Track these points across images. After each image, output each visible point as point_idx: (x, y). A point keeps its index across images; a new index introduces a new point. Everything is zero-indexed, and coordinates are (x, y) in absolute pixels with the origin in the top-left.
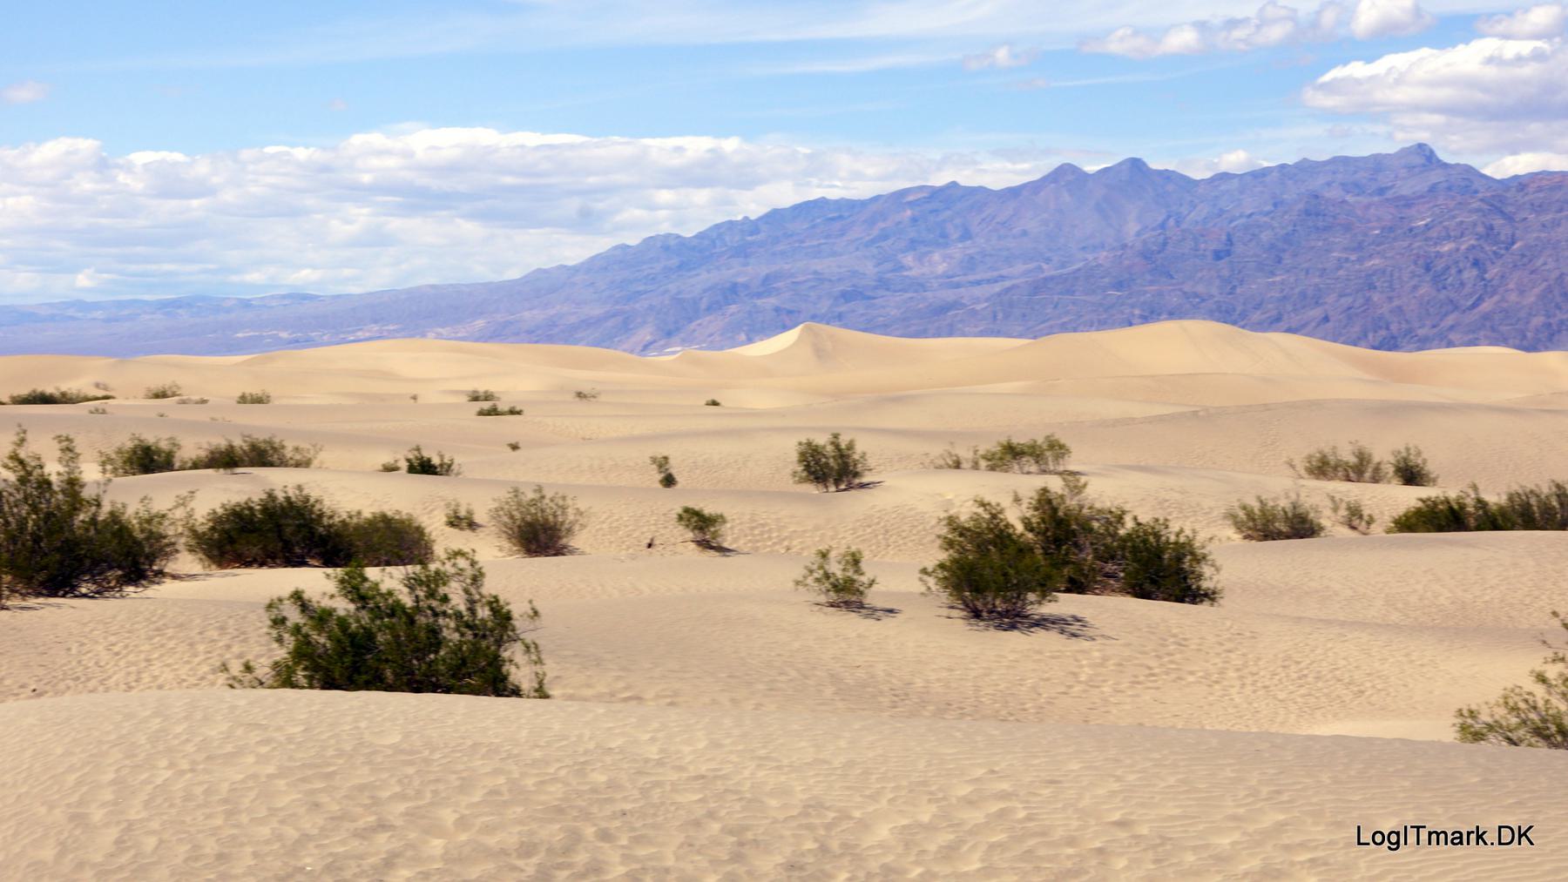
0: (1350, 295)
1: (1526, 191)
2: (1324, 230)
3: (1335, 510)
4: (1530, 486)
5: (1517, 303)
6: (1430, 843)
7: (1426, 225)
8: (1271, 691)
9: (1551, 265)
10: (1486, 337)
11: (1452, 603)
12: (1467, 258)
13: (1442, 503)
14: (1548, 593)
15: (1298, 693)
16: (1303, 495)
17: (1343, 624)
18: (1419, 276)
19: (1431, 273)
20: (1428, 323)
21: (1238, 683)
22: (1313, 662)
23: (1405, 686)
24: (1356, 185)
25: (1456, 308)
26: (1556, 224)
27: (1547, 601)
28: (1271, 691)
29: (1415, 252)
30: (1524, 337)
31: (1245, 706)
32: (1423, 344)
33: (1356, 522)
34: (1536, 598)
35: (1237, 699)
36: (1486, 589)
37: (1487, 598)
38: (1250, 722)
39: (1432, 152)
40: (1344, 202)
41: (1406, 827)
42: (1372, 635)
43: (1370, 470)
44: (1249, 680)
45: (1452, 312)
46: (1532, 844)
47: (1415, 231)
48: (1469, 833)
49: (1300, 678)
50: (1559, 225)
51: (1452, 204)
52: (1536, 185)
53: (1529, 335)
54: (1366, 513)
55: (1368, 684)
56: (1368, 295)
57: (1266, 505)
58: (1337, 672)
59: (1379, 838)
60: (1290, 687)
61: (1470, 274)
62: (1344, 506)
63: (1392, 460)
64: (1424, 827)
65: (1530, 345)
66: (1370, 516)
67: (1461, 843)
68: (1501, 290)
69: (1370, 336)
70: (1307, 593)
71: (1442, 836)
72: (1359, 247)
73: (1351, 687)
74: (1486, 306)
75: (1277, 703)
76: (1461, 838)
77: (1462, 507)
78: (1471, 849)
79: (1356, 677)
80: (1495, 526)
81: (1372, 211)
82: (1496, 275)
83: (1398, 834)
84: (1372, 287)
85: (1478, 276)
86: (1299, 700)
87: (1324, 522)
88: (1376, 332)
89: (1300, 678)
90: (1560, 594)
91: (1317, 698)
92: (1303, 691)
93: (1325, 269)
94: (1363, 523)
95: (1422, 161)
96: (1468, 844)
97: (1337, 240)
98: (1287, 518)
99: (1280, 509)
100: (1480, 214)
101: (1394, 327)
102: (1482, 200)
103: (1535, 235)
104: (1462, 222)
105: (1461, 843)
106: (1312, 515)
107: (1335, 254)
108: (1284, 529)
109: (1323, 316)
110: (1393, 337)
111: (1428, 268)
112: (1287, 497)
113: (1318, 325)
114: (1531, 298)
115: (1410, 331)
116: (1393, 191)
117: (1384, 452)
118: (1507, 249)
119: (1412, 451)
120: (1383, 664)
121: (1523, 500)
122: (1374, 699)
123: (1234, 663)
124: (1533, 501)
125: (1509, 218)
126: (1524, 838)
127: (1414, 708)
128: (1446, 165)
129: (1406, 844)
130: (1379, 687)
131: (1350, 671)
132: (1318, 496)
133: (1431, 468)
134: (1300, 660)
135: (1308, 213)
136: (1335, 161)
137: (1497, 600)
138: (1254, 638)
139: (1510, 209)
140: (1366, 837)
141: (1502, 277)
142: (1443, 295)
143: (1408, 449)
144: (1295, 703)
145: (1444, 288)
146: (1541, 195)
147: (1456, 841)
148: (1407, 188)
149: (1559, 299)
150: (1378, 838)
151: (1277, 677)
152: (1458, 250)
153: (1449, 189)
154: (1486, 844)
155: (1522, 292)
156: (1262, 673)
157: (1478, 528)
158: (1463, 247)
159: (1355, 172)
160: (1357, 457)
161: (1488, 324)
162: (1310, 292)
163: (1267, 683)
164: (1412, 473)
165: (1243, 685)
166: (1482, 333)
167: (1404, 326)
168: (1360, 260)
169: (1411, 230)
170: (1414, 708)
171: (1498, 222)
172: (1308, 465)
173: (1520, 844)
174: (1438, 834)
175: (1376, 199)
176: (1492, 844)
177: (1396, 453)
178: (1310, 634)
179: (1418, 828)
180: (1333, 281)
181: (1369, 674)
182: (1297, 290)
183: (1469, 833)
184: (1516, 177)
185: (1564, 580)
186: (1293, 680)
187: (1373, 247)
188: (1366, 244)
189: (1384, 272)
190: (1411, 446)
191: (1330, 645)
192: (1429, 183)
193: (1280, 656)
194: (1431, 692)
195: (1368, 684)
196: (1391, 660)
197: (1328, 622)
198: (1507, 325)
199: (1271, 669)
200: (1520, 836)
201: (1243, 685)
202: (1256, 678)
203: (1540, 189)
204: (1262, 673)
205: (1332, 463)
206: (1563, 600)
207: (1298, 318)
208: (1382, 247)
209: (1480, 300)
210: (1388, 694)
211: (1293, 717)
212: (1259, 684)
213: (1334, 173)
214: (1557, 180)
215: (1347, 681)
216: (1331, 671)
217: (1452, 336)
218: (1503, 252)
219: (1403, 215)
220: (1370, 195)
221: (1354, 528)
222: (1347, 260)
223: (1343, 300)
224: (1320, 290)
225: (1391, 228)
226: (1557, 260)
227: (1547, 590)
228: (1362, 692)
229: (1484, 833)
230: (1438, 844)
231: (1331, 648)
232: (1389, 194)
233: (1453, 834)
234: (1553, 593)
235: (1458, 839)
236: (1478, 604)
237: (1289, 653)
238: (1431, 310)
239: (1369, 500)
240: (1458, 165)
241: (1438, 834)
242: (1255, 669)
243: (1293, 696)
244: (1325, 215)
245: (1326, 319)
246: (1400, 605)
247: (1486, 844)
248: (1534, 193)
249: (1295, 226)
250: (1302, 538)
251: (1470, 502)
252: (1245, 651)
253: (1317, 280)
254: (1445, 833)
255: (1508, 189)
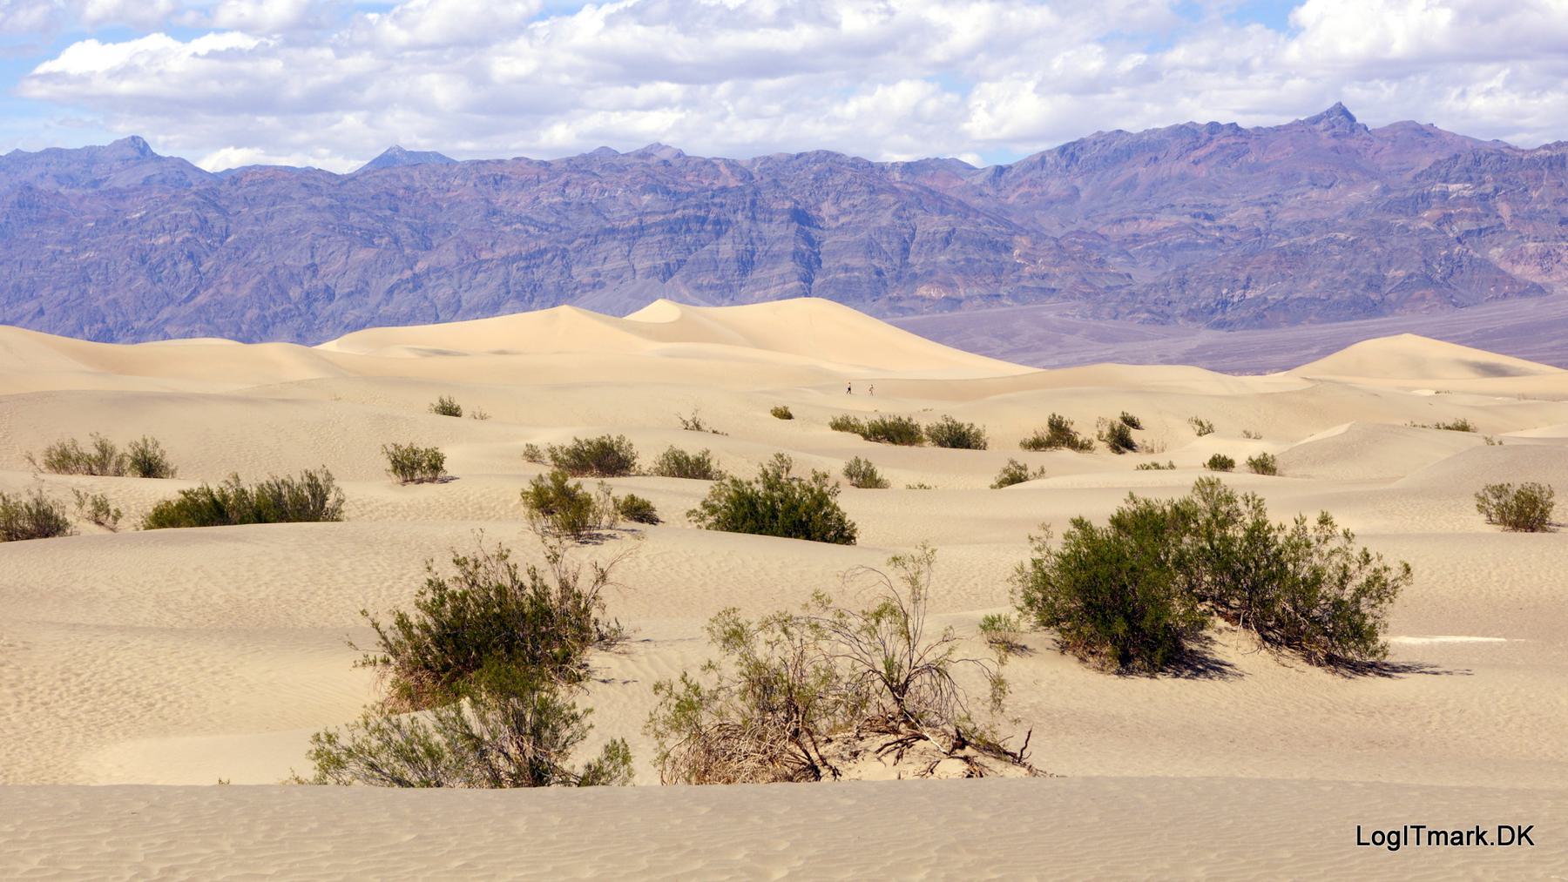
0: (66, 287)
1: (239, 185)
2: (38, 222)
3: (81, 505)
4: (282, 476)
5: (232, 295)
6: (1430, 843)
7: (141, 218)
8: (52, 708)
9: (264, 258)
10: (201, 330)
11: (226, 601)
12: (182, 251)
13: (204, 494)
14: (324, 587)
15: (83, 709)
16: (44, 490)
17: (122, 629)
18: (135, 269)
19: (147, 265)
20: (144, 315)
21: (14, 701)
22: (95, 674)
23: (198, 696)
24: (70, 177)
25: (171, 300)
26: (269, 217)
27: (324, 596)
28: (52, 708)
29: (130, 244)
30: (240, 329)
31: (25, 726)
32: (139, 336)
33: (102, 518)
34: (312, 593)
35: (13, 719)
36: (260, 586)
37: (262, 595)
38: (32, 745)
39: (146, 145)
40: (58, 193)
41: (1406, 827)
42: (156, 641)
43: (113, 463)
44: (25, 698)
45: (168, 304)
46: (1532, 844)
47: (130, 223)
48: (1469, 833)
49: (82, 692)
50: (272, 218)
51: (167, 197)
52: (248, 179)
53: (244, 327)
54: (112, 508)
55: (158, 696)
56: (83, 287)
57: (9, 501)
58: (123, 684)
59: (1379, 838)
60: (72, 703)
61: (185, 267)
62: (89, 501)
63: (130, 452)
64: (1424, 827)
65: (249, 336)
66: (118, 512)
67: (1461, 843)
68: (216, 283)
69: (86, 330)
70: (71, 596)
71: (1442, 836)
72: (75, 240)
73: (139, 700)
74: (202, 298)
75: (60, 721)
76: (1461, 838)
77: (225, 498)
78: (1473, 847)
79: (144, 689)
80: (260, 519)
81: (87, 203)
82: (211, 267)
83: (1398, 834)
84: (86, 280)
85: (192, 269)
86: (83, 716)
87: (69, 518)
88: (92, 325)
89: (82, 692)
90: (336, 589)
91: (103, 713)
92: (86, 707)
93: (39, 262)
94: (110, 518)
95: (136, 154)
96: (1468, 844)
97: (51, 232)
98: (31, 514)
99: (23, 505)
100: (194, 207)
101: (110, 321)
102: (196, 193)
103: (248, 229)
104: (176, 215)
105: (1461, 843)
106: (56, 511)
107: (49, 247)
108: (28, 526)
109: (38, 309)
110: (109, 330)
111: (143, 262)
112: (30, 493)
113: (34, 317)
114: (245, 291)
115: (127, 323)
116: (108, 183)
117: (123, 443)
118: (221, 242)
119: (149, 442)
120: (172, 673)
121: (274, 492)
122: (166, 712)
123: (7, 678)
124: (285, 491)
125: (223, 211)
126: (1524, 838)
127: (210, 721)
128: (160, 158)
129: (1406, 844)
130: (169, 699)
131: (136, 682)
132: (62, 491)
133: (169, 459)
134: (80, 672)
135: (21, 205)
136: (48, 152)
137: (272, 598)
138: (28, 649)
139: (224, 202)
140: (1366, 838)
141: (217, 270)
142: (159, 288)
143: (145, 441)
144: (80, 720)
145: (160, 280)
146: (255, 189)
147: (1456, 841)
148: (122, 180)
149: (272, 291)
150: (1378, 838)
151: (57, 692)
152: (173, 243)
153: (163, 181)
154: (1485, 844)
155: (236, 285)
156: (40, 689)
157: (243, 521)
158: (178, 240)
159: (69, 164)
160: (99, 450)
161: (203, 317)
162: (25, 285)
163: (46, 700)
164: (150, 465)
165: (20, 703)
166: (197, 326)
167: (120, 319)
168: (75, 253)
169: (126, 222)
170: (210, 721)
171: (212, 215)
172: (47, 458)
173: (1520, 844)
174: (1438, 834)
175: (90, 191)
176: (1492, 844)
177: (133, 445)
178: (89, 642)
179: (1418, 828)
180: (48, 274)
181: (158, 685)
182: (11, 283)
183: (1469, 833)
184: (229, 171)
185: (339, 574)
186: (75, 695)
187: (87, 240)
188: (80, 236)
189: (99, 265)
190: (148, 438)
191: (111, 654)
192: (144, 176)
193: (59, 667)
194: (227, 703)
195: (158, 696)
196: (180, 668)
197: (107, 628)
198: (221, 318)
199: (51, 683)
200: (1520, 836)
201: (20, 703)
202: (33, 694)
203: (252, 183)
204: (40, 689)
205: (73, 457)
206: (341, 595)
207: (12, 311)
208: (98, 239)
209: (195, 292)
210: (180, 706)
211: (80, 736)
212: (38, 701)
213: (47, 165)
214: (268, 174)
215: (134, 693)
216: (116, 683)
217: (167, 329)
218: (217, 245)
219: (116, 208)
220: (85, 187)
221: (100, 523)
222: (61, 252)
223: (58, 293)
224: (34, 282)
225: (105, 220)
226: (271, 253)
227: (322, 585)
228: (152, 705)
229: (1484, 833)
230: (1438, 844)
231: (114, 658)
232: (103, 187)
233: (1453, 834)
234: (329, 588)
235: (1458, 839)
236: (253, 601)
237: (68, 664)
238: (147, 304)
239: (115, 493)
240: (171, 158)
241: (1438, 834)
242: (31, 684)
243: (76, 713)
244: (38, 207)
245: (41, 312)
246: (172, 606)
247: (1485, 844)
248: (247, 186)
249: (8, 218)
250: (47, 536)
251: (230, 492)
252: (19, 664)
253: (31, 273)
254: (1445, 833)
255: (221, 183)
